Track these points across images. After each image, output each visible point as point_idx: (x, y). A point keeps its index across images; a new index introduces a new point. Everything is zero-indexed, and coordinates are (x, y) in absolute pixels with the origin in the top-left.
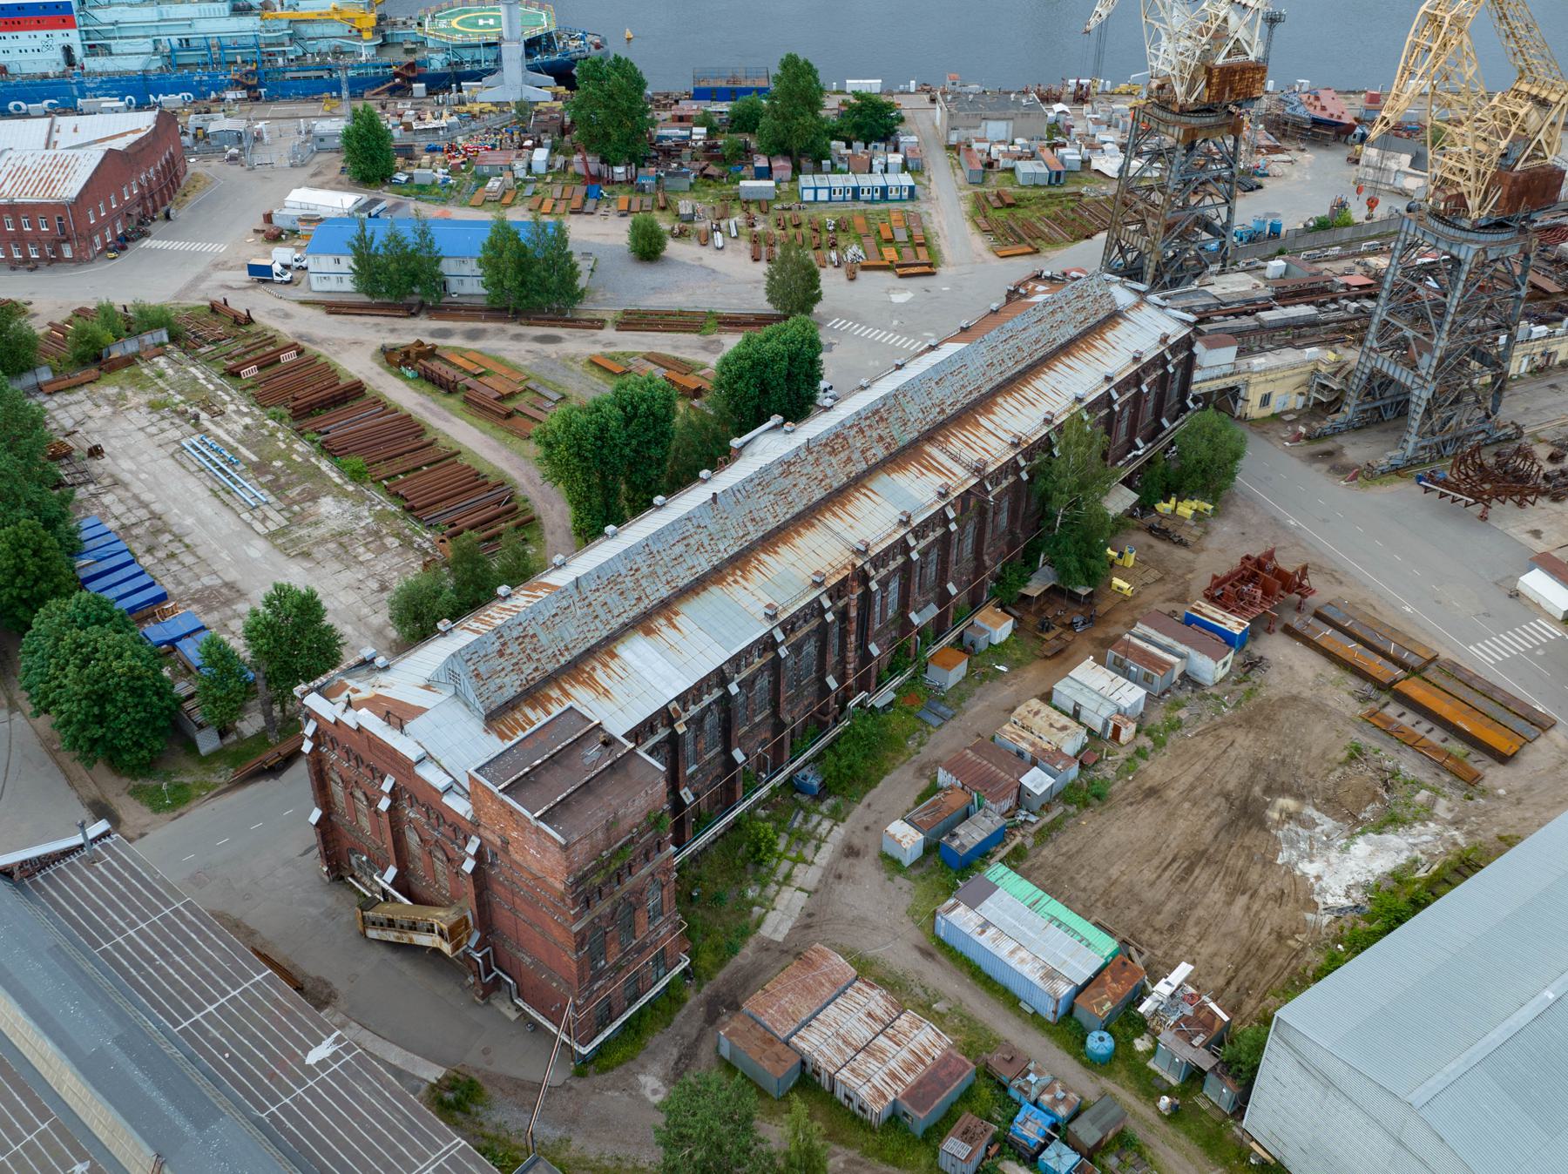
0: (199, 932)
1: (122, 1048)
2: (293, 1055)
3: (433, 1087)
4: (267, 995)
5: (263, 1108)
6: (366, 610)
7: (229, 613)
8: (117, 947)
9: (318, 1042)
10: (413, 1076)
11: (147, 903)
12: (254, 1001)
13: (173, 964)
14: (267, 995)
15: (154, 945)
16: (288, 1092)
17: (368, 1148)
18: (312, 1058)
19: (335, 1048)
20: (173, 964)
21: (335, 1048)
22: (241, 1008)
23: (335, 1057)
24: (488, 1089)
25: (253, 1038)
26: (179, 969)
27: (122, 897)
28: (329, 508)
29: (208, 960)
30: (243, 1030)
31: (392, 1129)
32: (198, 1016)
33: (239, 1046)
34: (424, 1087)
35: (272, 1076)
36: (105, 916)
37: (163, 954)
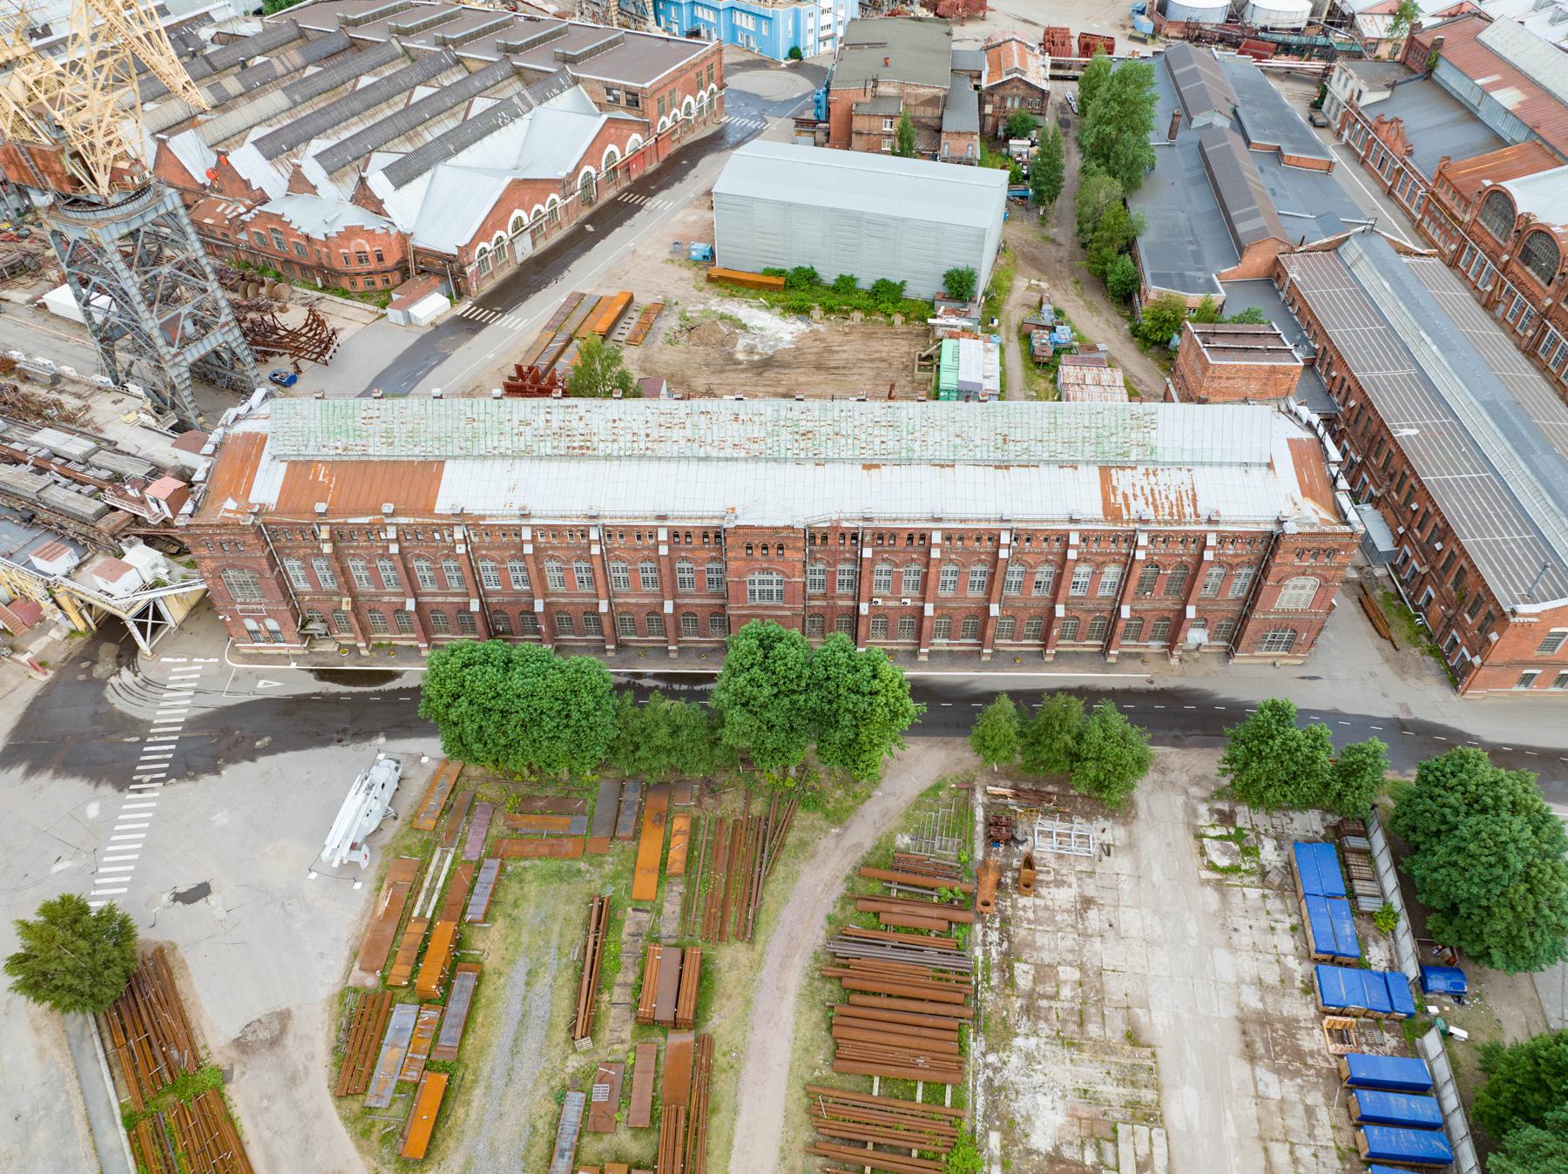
4: (1429, 468)
6: (1126, 886)
7: (1270, 999)
8: (1519, 533)
9: (1408, 437)
11: (1492, 551)
14: (1429, 468)
15: (1493, 524)
18: (1415, 432)
23: (1402, 427)
25: (1445, 453)
26: (1480, 504)
27: (1510, 563)
28: (1049, 1114)
29: (1459, 501)
33: (1454, 453)
36: (1524, 555)
37: (1488, 516)
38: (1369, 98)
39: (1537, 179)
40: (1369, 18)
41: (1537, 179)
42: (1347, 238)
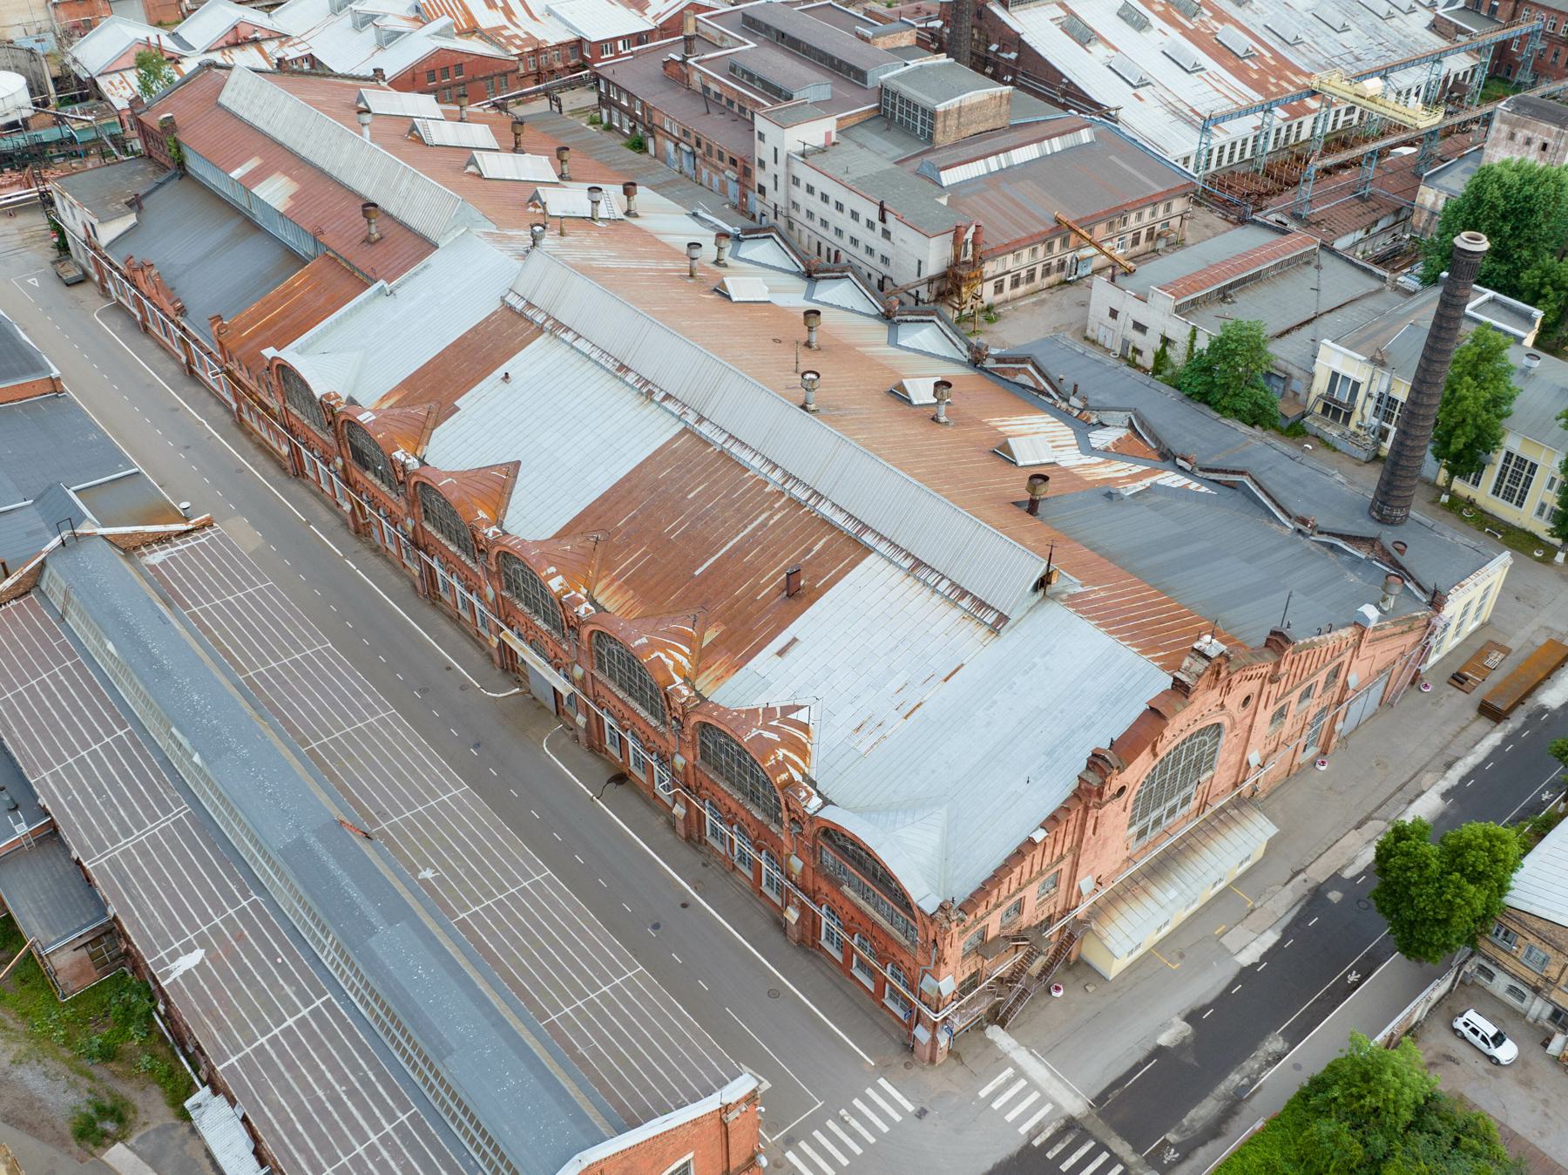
0: (293, 1134)
1: (370, 924)
2: (215, 959)
3: (123, 1139)
4: (228, 1036)
5: (254, 905)
9: (187, 975)
10: (140, 1155)
12: (242, 1027)
13: (327, 1086)
15: (348, 1117)
16: (228, 921)
17: (169, 864)
18: (199, 954)
19: (171, 966)
20: (327, 1086)
21: (171, 966)
22: (258, 1020)
23: (174, 956)
24: (67, 1130)
25: (252, 983)
26: (320, 1079)
29: (287, 1091)
30: (259, 992)
31: (144, 880)
32: (305, 1012)
34: (132, 1141)
35: (240, 938)
38: (107, 233)
39: (338, 322)
40: (116, 78)
41: (338, 322)
42: (43, 563)
